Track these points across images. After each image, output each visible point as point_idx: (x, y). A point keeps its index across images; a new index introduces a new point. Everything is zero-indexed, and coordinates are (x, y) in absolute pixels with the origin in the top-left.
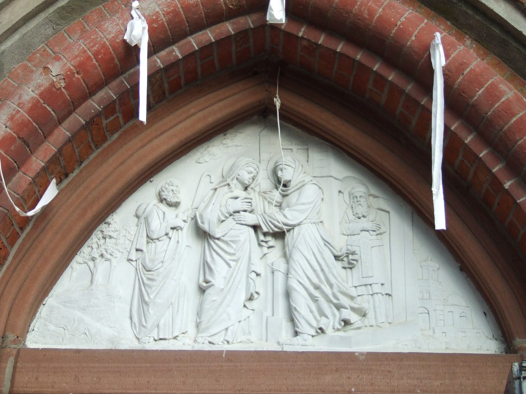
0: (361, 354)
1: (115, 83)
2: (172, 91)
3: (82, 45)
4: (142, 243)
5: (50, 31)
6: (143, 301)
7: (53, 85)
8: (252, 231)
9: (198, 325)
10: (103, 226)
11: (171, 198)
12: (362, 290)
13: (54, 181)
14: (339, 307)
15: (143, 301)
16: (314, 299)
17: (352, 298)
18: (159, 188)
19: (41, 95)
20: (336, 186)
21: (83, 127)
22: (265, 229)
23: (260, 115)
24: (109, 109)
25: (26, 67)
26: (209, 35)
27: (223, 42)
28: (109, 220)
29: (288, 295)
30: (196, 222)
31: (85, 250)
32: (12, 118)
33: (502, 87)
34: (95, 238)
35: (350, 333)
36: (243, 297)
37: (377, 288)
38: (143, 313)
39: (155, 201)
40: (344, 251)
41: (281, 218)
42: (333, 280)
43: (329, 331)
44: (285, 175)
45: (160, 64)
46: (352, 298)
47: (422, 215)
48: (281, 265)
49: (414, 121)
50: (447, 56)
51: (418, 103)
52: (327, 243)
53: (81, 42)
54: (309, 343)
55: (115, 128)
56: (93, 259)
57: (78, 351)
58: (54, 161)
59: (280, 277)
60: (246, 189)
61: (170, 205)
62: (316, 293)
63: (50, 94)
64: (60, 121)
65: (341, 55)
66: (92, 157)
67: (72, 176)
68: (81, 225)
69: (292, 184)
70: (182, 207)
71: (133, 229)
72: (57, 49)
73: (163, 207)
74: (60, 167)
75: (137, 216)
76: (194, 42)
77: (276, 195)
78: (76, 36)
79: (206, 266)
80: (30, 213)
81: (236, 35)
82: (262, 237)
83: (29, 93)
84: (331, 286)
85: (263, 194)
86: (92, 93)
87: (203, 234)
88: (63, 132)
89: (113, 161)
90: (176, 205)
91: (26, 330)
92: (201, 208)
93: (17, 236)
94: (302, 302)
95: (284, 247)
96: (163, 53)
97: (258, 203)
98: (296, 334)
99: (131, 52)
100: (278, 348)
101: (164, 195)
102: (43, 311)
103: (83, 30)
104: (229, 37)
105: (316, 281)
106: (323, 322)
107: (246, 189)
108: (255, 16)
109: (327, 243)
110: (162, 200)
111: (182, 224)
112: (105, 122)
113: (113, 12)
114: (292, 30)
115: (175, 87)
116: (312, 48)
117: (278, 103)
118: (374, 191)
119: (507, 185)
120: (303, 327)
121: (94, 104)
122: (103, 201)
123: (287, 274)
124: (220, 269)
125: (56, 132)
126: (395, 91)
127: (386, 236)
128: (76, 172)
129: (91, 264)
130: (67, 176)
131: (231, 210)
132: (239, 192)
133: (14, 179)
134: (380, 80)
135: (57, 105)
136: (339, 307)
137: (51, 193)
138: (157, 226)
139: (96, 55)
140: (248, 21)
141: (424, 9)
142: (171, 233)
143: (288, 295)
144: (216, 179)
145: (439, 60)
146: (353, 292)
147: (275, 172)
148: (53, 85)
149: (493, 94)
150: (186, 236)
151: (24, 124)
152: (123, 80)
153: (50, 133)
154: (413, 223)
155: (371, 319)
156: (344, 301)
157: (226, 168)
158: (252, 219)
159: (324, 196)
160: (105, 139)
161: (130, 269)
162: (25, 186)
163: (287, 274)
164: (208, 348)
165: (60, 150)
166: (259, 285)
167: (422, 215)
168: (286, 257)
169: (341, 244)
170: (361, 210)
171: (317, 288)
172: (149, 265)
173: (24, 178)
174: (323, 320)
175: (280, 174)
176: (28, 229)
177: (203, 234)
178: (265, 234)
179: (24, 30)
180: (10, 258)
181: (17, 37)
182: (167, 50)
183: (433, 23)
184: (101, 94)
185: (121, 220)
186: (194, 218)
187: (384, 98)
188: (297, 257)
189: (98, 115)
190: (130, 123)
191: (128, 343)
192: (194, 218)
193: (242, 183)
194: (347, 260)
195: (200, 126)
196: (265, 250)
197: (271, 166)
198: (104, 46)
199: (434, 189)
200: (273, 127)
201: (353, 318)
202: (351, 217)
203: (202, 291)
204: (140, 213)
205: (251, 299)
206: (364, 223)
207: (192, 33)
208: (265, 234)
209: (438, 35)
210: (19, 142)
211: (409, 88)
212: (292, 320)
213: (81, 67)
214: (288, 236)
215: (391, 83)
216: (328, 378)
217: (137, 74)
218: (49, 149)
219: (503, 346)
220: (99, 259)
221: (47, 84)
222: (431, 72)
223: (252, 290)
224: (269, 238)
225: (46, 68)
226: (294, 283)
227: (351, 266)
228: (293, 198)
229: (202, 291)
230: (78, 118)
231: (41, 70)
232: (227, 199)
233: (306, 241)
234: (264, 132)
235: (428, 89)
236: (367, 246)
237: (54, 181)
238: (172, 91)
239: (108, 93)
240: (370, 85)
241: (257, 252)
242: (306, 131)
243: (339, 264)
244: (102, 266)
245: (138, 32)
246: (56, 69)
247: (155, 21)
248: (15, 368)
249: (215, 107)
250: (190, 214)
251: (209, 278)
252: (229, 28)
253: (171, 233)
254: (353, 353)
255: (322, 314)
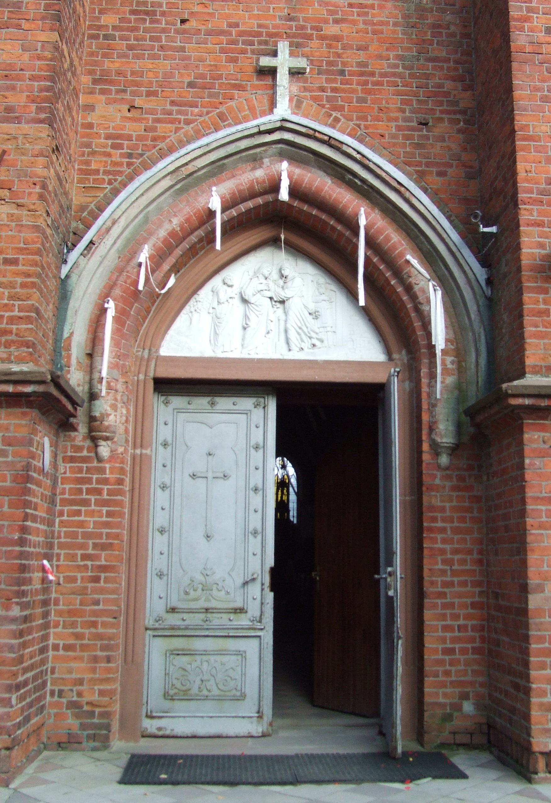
0: (321, 361)
1: (203, 228)
2: (231, 230)
3: (188, 209)
4: (215, 304)
5: (171, 201)
6: (216, 333)
7: (174, 229)
8: (269, 300)
9: (242, 345)
10: (196, 296)
11: (230, 284)
12: (322, 330)
13: (173, 275)
14: (310, 338)
15: (216, 333)
16: (299, 334)
17: (317, 333)
18: (223, 277)
19: (168, 234)
20: (310, 278)
21: (188, 249)
22: (275, 299)
23: (274, 242)
24: (201, 240)
25: (159, 219)
26: (250, 204)
27: (257, 208)
28: (198, 293)
29: (286, 331)
30: (242, 295)
31: (187, 308)
32: (154, 246)
33: (392, 235)
34: (192, 302)
35: (315, 350)
36: (265, 332)
37: (329, 329)
38: (216, 339)
39: (221, 284)
40: (314, 311)
41: (283, 294)
42: (308, 325)
43: (306, 349)
44: (285, 273)
45: (226, 219)
46: (317, 333)
47: (353, 295)
48: (283, 317)
49: (349, 249)
50: (367, 219)
51: (351, 241)
52: (305, 307)
53: (187, 207)
54: (296, 355)
55: (203, 248)
56: (191, 312)
57: (186, 357)
58: (174, 266)
59: (282, 323)
60: (266, 279)
61: (229, 286)
62: (300, 331)
63: (172, 234)
64: (177, 247)
65: (315, 216)
66: (191, 262)
67: (181, 272)
68: (186, 296)
69: (289, 277)
70: (234, 288)
71: (211, 297)
72: (175, 210)
73: (225, 287)
74: (176, 269)
75: (213, 291)
76: (242, 207)
77: (281, 282)
78: (184, 203)
79: (246, 317)
80: (163, 291)
81: (263, 204)
82: (274, 303)
83: (162, 233)
84: (307, 328)
85: (275, 281)
86: (192, 232)
87: (245, 301)
88: (178, 252)
89: (201, 264)
90: (231, 286)
91: (159, 346)
92: (244, 288)
93: (155, 301)
94: (293, 335)
95: (284, 309)
96: (227, 213)
97: (272, 286)
98: (290, 350)
99: (211, 214)
100: (281, 357)
101: (226, 281)
102: (167, 337)
103: (188, 201)
104: (260, 205)
105: (300, 325)
106: (303, 345)
107: (266, 279)
108: (273, 195)
109: (305, 307)
110: (224, 284)
111: (235, 296)
112: (198, 246)
113: (203, 192)
114: (291, 203)
115: (232, 228)
116: (301, 211)
117: (283, 237)
118: (328, 281)
119: (393, 282)
120: (293, 347)
121: (193, 238)
122: (197, 284)
123: (286, 321)
124: (252, 316)
125: (175, 252)
126: (341, 234)
127: (334, 303)
128: (183, 270)
129: (190, 314)
130: (179, 272)
131: (259, 289)
132: (262, 280)
133: (155, 275)
134: (333, 229)
135: (177, 238)
136: (310, 338)
137: (172, 282)
138: (223, 297)
139: (195, 214)
140: (269, 198)
141: (356, 194)
142: (229, 300)
143: (286, 331)
144: (251, 273)
145: (363, 222)
146: (317, 331)
147: (280, 271)
148: (174, 229)
149: (388, 239)
150: (237, 301)
151: (161, 249)
152: (208, 226)
153: (172, 252)
154: (347, 298)
155: (325, 343)
156: (313, 335)
157: (257, 268)
158: (269, 294)
159: (304, 283)
160: (197, 254)
161: (210, 317)
162: (160, 278)
163: (286, 321)
164: (247, 356)
165: (177, 261)
166: (272, 326)
167: (353, 295)
168: (286, 313)
169: (312, 307)
170: (322, 290)
171: (300, 328)
172: (219, 316)
173: (160, 274)
174: (303, 344)
175: (283, 272)
176: (160, 298)
177: (245, 301)
178: (275, 302)
179: (158, 201)
180: (152, 312)
181: (155, 204)
182: (229, 211)
183: (360, 202)
184: (196, 233)
185: (205, 293)
186: (241, 293)
187: (335, 236)
188: (291, 313)
189: (195, 244)
190: (210, 246)
191: (208, 353)
192: (241, 293)
193: (264, 276)
194: (315, 315)
195: (244, 248)
196: (275, 309)
197: (279, 267)
198: (199, 210)
199: (359, 286)
200: (280, 248)
201: (317, 343)
202: (317, 294)
203: (245, 329)
204: (214, 289)
205: (268, 333)
206: (323, 297)
207: (241, 203)
208: (275, 302)
209: (362, 210)
210: (158, 257)
211: (348, 233)
212: (288, 343)
213: (188, 220)
214: (287, 303)
215: (339, 231)
216: (305, 372)
217: (215, 224)
218: (171, 260)
219: (387, 358)
220: (194, 312)
221: (171, 229)
222: (358, 227)
223: (269, 329)
224: (277, 304)
225: (170, 220)
226: (289, 326)
227: (316, 318)
228: (289, 284)
229: (245, 329)
230: (186, 245)
231: (167, 221)
232: (256, 284)
233: (294, 305)
234: (275, 250)
235: (357, 234)
236: (326, 310)
237: (173, 275)
238: (231, 230)
239: (201, 233)
240: (328, 230)
241: (271, 310)
242: (295, 250)
243: (311, 317)
244: (195, 315)
245: (216, 204)
246: (175, 221)
247: (224, 198)
248: (156, 365)
249: (251, 238)
250: (239, 290)
251: (248, 322)
252: (260, 201)
253: (229, 300)
254: (316, 361)
255: (302, 341)
